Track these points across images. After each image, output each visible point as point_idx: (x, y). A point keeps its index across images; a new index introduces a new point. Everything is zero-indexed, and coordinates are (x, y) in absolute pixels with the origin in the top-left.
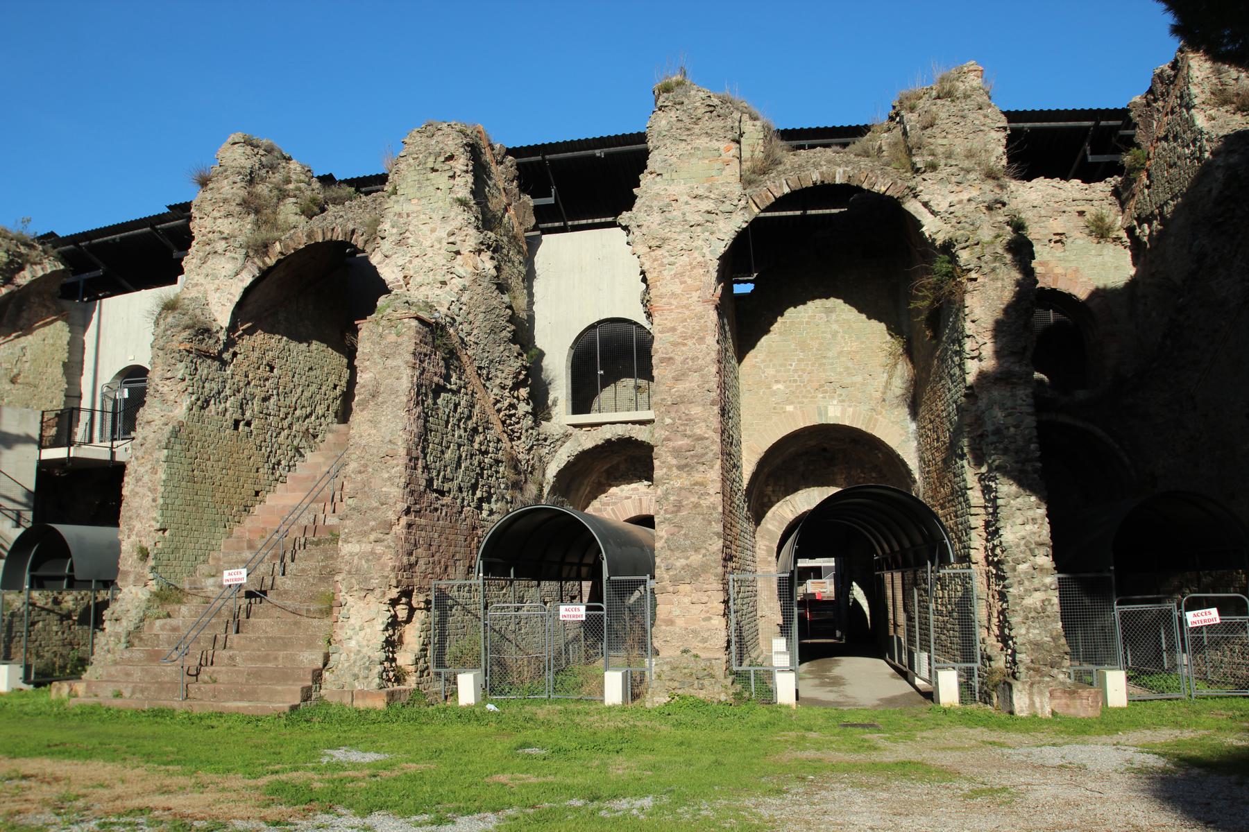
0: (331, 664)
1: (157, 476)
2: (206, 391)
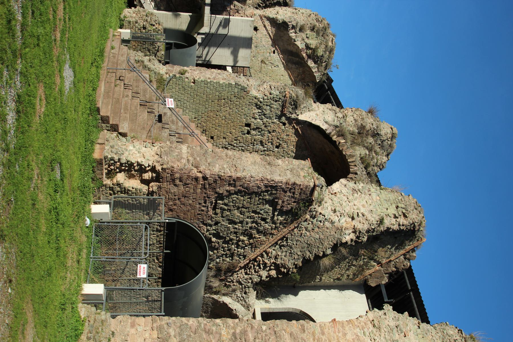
0: (120, 137)
1: (221, 80)
2: (265, 107)
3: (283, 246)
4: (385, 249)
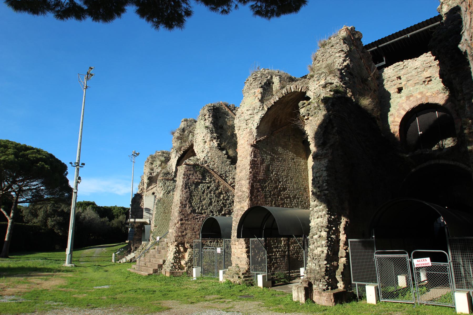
2: (169, 189)
3: (226, 176)
4: (228, 121)
